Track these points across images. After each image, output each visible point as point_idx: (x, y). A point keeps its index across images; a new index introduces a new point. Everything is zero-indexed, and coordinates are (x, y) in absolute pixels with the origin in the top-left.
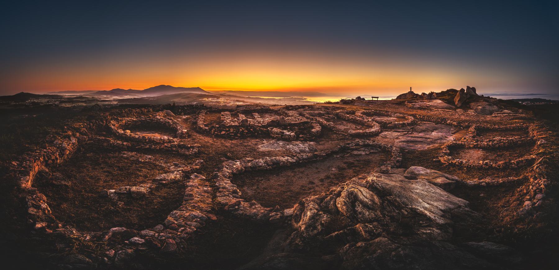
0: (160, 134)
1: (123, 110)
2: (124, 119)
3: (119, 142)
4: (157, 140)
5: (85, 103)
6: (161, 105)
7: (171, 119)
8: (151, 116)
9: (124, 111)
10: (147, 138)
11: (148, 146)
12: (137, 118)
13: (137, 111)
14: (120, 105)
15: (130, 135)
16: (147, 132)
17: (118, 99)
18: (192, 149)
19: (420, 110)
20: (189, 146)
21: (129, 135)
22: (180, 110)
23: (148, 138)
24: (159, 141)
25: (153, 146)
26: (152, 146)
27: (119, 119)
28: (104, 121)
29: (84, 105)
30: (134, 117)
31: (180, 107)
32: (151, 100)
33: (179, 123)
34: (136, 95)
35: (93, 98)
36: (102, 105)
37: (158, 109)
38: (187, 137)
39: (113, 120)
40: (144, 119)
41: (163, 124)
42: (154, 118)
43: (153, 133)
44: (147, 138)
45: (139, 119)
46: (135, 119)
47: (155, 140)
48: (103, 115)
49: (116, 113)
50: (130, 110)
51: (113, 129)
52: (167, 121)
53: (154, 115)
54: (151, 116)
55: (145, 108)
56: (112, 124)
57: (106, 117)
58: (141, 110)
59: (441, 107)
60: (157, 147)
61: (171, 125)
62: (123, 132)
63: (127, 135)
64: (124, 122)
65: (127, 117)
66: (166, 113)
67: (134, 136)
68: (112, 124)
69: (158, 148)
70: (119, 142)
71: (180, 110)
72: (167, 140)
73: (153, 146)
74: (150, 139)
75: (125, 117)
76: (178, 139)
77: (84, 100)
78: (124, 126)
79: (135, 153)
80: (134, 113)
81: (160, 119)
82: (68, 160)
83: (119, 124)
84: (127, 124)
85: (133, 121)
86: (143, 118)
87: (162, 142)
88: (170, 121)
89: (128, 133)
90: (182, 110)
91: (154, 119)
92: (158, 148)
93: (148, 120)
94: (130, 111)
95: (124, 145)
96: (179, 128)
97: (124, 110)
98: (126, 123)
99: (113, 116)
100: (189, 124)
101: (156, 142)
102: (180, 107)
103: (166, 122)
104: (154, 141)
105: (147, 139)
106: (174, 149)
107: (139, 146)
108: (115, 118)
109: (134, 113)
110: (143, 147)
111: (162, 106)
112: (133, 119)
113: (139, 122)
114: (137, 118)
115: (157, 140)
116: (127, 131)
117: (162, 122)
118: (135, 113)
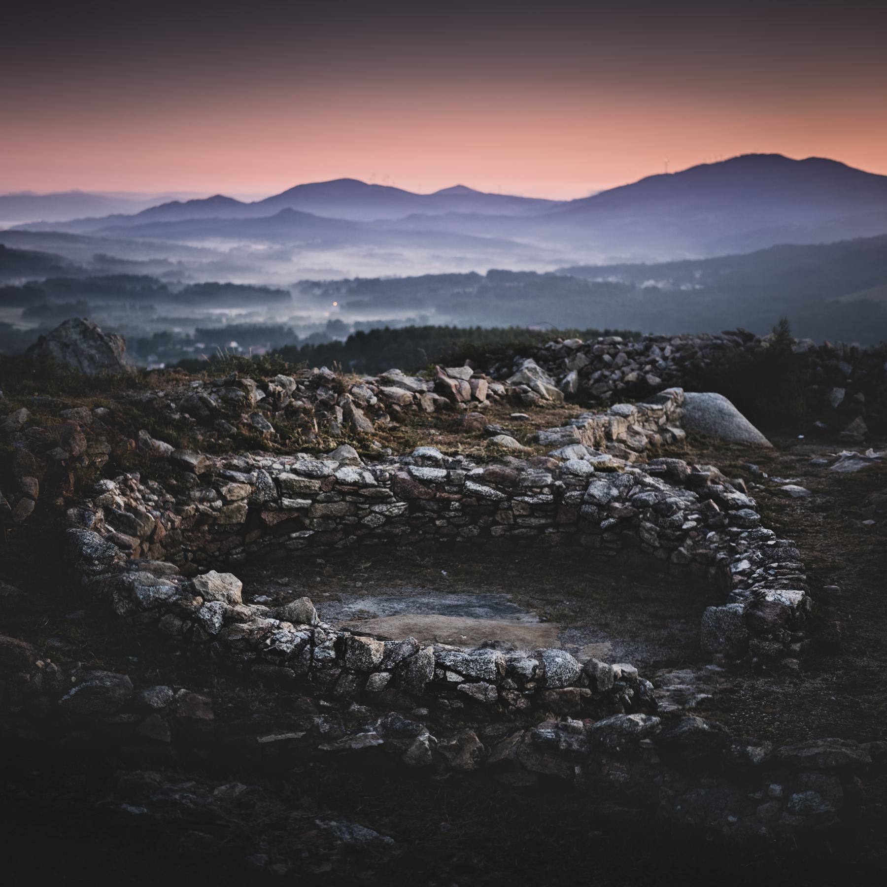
0: (559, 618)
1: (249, 382)
2: (248, 469)
3: (105, 678)
4: (468, 679)
5: (28, 315)
6: (662, 339)
7: (694, 482)
8: (508, 441)
9: (257, 395)
10: (377, 658)
11: (372, 737)
12: (379, 458)
13: (398, 399)
14: (360, 334)
15: (231, 619)
16: (451, 600)
17: (347, 281)
18: (777, 788)
19: (329, 647)
20: (757, 753)
21: (217, 621)
22: (840, 393)
23: (388, 654)
24: (492, 695)
25: (425, 737)
26: (414, 735)
27: (190, 467)
28: (28, 480)
29: (24, 326)
30: (350, 452)
31: (847, 368)
32: (648, 289)
33: (754, 524)
34: (507, 246)
35: (101, 259)
36: (192, 332)
37: (632, 376)
38: (794, 663)
39: (134, 480)
40: (441, 473)
41: (611, 527)
42: (536, 464)
43: (498, 610)
44: (377, 658)
45: (389, 469)
46: (350, 474)
47: (452, 677)
48: (31, 422)
49: (182, 409)
50: (319, 382)
51: (89, 560)
52: (649, 497)
53: (542, 434)
54: (508, 441)
55: (481, 367)
56: (108, 511)
57: (54, 444)
58: (441, 388)
59: (449, 636)
60: (459, 749)
61: (681, 540)
62: (167, 586)
63: (202, 623)
64: (240, 491)
65: (278, 453)
66: (684, 422)
67: (267, 631)
68: (108, 511)
69: (468, 760)
70: (105, 678)
71: (840, 393)
72: (577, 682)
73: (425, 737)
74: (406, 663)
75: (256, 446)
76: (707, 679)
77: (19, 282)
78: (243, 530)
79: (240, 788)
80: (358, 413)
81: (586, 481)
82: (666, 775)
83: (190, 508)
84: (268, 517)
85: (335, 485)
86: (435, 463)
87: (522, 703)
88: (681, 499)
89: (208, 597)
90: (861, 397)
91: (531, 473)
92: (468, 760)
93: (478, 479)
94: (322, 394)
95: (149, 709)
96: (744, 565)
97: (263, 387)
98: (256, 507)
99: (143, 434)
100: (870, 530)
101: (463, 696)
102: (847, 368)
103: (645, 504)
104: (441, 684)
105: (377, 669)
106: (619, 774)
107: (294, 728)
108: (161, 458)
109: (358, 413)
110: (328, 738)
111: (668, 349)
112: (329, 466)
113: (383, 499)
114: (370, 457)
115: (468, 679)
116: (213, 579)
117: (604, 507)
118: (371, 411)
